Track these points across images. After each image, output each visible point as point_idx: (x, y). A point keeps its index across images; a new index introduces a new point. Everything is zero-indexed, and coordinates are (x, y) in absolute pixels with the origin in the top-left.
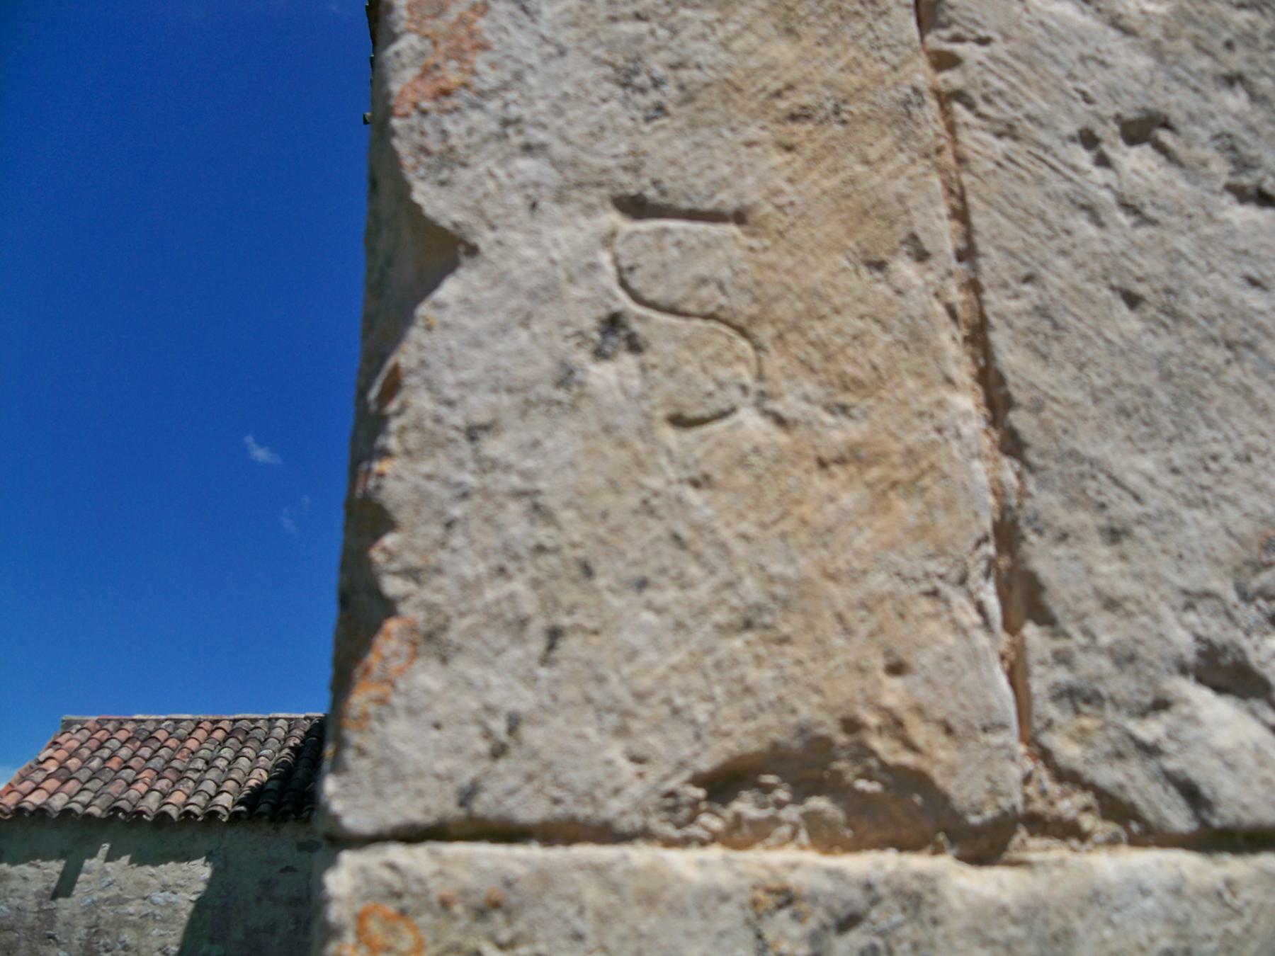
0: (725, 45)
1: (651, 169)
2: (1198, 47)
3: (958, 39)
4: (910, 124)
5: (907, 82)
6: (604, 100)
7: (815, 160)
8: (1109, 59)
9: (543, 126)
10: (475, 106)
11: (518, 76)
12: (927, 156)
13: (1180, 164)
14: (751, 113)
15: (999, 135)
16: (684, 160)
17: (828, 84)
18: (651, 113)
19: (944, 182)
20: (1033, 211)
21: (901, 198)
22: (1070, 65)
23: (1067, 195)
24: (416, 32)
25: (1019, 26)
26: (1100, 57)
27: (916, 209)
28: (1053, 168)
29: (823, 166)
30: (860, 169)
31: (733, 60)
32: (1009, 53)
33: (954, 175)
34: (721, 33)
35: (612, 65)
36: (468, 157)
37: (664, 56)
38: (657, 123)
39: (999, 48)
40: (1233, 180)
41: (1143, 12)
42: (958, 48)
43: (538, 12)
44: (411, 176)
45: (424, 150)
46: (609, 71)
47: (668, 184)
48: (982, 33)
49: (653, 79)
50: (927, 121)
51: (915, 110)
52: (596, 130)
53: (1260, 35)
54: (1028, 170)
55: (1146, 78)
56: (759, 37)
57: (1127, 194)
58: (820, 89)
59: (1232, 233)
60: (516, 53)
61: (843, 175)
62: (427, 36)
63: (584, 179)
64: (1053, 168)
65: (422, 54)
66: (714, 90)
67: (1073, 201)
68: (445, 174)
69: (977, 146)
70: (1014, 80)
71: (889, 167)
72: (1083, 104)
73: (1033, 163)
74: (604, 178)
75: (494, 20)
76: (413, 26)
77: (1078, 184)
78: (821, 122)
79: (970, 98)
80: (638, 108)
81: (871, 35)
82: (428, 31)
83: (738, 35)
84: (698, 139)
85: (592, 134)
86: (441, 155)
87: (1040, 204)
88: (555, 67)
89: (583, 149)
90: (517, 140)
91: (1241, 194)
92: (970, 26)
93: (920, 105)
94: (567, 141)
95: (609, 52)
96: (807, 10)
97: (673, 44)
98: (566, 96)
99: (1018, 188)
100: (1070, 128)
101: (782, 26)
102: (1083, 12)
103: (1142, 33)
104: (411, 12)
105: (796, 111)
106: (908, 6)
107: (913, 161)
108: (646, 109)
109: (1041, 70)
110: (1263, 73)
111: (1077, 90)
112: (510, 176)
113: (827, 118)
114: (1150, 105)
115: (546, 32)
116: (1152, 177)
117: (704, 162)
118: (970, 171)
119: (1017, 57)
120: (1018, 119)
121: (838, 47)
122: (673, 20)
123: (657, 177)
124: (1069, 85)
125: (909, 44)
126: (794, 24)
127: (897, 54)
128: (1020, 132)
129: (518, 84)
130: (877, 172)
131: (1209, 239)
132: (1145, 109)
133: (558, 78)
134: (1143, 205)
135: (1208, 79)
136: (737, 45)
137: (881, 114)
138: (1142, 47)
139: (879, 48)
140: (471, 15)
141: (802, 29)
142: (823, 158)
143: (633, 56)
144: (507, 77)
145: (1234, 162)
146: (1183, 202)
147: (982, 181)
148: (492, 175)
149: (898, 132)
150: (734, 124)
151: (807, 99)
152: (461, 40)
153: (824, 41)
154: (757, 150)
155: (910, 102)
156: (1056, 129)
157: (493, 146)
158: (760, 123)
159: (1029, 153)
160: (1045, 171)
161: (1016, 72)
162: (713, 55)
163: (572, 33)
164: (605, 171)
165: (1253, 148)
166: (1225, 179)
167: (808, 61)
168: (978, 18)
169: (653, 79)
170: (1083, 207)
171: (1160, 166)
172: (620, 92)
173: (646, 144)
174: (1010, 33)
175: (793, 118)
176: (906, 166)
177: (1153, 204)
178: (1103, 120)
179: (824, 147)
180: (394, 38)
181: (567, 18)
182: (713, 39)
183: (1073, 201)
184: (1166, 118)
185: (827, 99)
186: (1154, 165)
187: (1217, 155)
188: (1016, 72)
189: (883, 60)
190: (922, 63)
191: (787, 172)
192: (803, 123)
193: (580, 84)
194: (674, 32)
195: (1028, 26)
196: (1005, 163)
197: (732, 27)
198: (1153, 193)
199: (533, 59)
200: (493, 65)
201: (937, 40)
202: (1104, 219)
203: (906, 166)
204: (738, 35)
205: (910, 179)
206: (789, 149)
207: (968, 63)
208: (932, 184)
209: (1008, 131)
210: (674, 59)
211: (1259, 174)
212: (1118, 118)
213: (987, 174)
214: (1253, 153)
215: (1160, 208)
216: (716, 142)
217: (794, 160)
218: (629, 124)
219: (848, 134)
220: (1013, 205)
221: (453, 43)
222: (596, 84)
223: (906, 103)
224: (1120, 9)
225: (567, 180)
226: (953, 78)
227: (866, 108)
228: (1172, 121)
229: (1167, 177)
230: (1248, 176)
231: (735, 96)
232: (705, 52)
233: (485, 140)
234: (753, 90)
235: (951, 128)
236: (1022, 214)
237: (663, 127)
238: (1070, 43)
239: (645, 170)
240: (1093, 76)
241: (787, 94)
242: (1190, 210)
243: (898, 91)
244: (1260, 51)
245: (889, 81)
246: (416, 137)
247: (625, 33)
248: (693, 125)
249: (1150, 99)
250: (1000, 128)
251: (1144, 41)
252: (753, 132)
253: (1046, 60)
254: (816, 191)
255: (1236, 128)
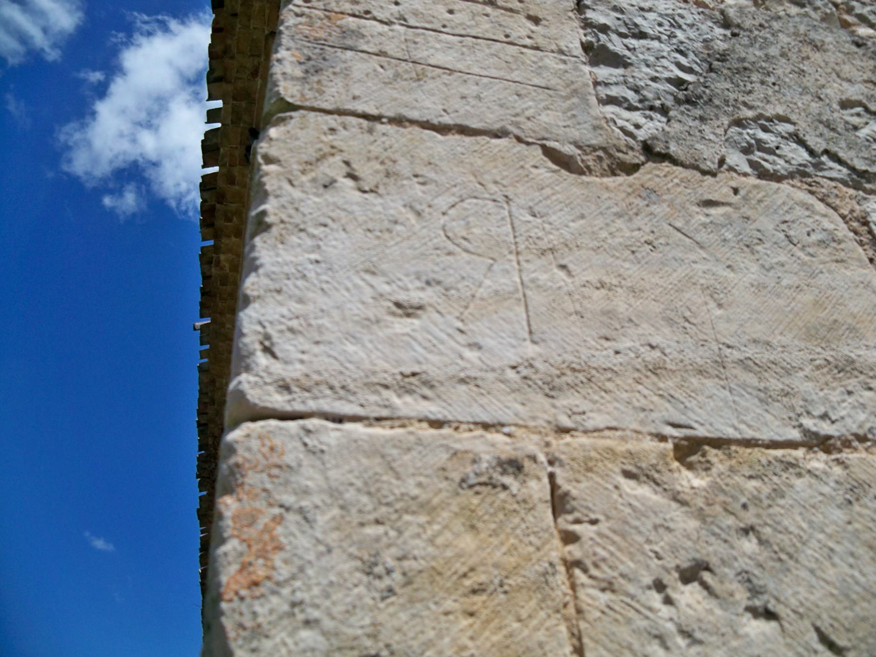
0: (431, 541)
1: (386, 635)
2: (726, 510)
3: (578, 521)
4: (547, 588)
5: (546, 559)
6: (356, 586)
7: (488, 621)
8: (671, 525)
9: (317, 606)
10: (274, 593)
11: (301, 569)
12: (558, 611)
13: (717, 597)
14: (448, 591)
15: (603, 590)
16: (405, 628)
17: (496, 566)
18: (385, 594)
19: (568, 628)
20: (625, 644)
21: (541, 645)
22: (648, 533)
23: (646, 630)
24: (237, 537)
25: (616, 508)
26: (666, 524)
27: (551, 651)
28: (637, 611)
29: (492, 625)
30: (516, 625)
31: (436, 552)
32: (610, 529)
33: (574, 622)
34: (429, 532)
35: (361, 559)
36: (269, 630)
37: (394, 551)
38: (389, 601)
39: (603, 527)
40: (750, 603)
41: (693, 488)
42: (577, 528)
43: (315, 521)
44: (233, 645)
45: (242, 626)
46: (358, 563)
47: (395, 647)
48: (593, 516)
49: (386, 569)
50: (558, 586)
51: (550, 579)
52: (350, 608)
53: (763, 497)
54: (621, 614)
55: (694, 536)
56: (453, 533)
57: (683, 624)
58: (491, 569)
59: (749, 644)
60: (300, 552)
61: (504, 632)
62: (244, 541)
63: (342, 645)
64: (637, 611)
65: (241, 554)
66: (425, 575)
67: (649, 633)
68: (254, 644)
69: (590, 601)
70: (612, 548)
71: (534, 622)
72: (656, 560)
73: (624, 608)
74: (355, 643)
75: (286, 527)
76: (236, 533)
77: (652, 620)
78: (491, 594)
79: (585, 565)
80: (376, 590)
81: (523, 526)
82: (245, 537)
83: (439, 533)
84: (414, 611)
85: (347, 612)
86: (253, 630)
87: (629, 639)
88: (325, 561)
89: (342, 622)
90: (300, 617)
91: (755, 612)
92: (585, 511)
93: (553, 574)
94: (333, 618)
95: (359, 549)
96: (484, 511)
97: (399, 541)
98: (331, 584)
99: (614, 628)
100: (648, 580)
101: (468, 523)
102: (656, 493)
103: (692, 503)
104: (235, 522)
105: (476, 587)
106: (546, 502)
107: (549, 616)
108: (382, 591)
109: (629, 540)
110: (766, 524)
111: (652, 551)
112: (296, 644)
113: (495, 590)
114: (698, 556)
115: (319, 535)
116: (699, 607)
117: (418, 629)
118: (584, 619)
119: (614, 532)
120: (614, 578)
121: (503, 536)
122: (399, 524)
123: (388, 641)
124: (647, 547)
125: (547, 530)
126: (475, 522)
127: (540, 538)
128: (616, 587)
129: (301, 575)
130: (527, 626)
131: (735, 650)
132: (694, 559)
133: (326, 570)
134: (693, 630)
135: (733, 532)
136: (439, 541)
137: (529, 584)
138: (692, 513)
139: (528, 535)
140: (272, 525)
141: (480, 525)
142: (493, 620)
143: (373, 552)
144: (295, 570)
145: (750, 590)
146: (719, 625)
147: (592, 626)
148: (285, 644)
149: (539, 596)
150: (437, 599)
151: (483, 578)
152: (265, 544)
153: (495, 533)
154: (451, 617)
155: (547, 573)
156: (639, 581)
157: (285, 622)
158: (453, 597)
159: (622, 601)
160: (632, 614)
161: (614, 543)
162: (424, 549)
163: (335, 535)
164: (356, 638)
165: (762, 579)
166: (745, 603)
167: (484, 549)
168: (590, 505)
169: (386, 569)
170: (656, 637)
171: (704, 598)
172: (365, 579)
173: (381, 618)
174: (610, 514)
175: (474, 592)
176: (545, 620)
177: (700, 628)
178: (668, 571)
179: (493, 612)
180: (223, 541)
181: (333, 524)
182: (424, 536)
183: (649, 633)
184: (708, 564)
185: (496, 577)
186: (700, 598)
187: (739, 586)
188: (614, 543)
189: (531, 543)
190: (557, 542)
191: (470, 633)
192: (480, 595)
193: (340, 574)
194: (400, 532)
195: (622, 508)
196: (607, 610)
197: (436, 527)
198: (700, 620)
199: (311, 556)
200: (286, 562)
201: (565, 522)
202: (669, 644)
203: (545, 620)
204: (439, 533)
205: (547, 629)
206: (472, 614)
207: (584, 539)
208: (560, 632)
209: (609, 587)
210: (400, 553)
211: (765, 597)
212: (678, 568)
213: (595, 620)
214: (761, 583)
215: (705, 631)
216: (425, 613)
217: (474, 623)
218: (371, 602)
219: (508, 600)
220: (612, 641)
221: (260, 546)
222: (351, 573)
223: (545, 574)
224: (679, 488)
225: (331, 645)
226: (575, 551)
227: (520, 580)
228: (711, 566)
229: (708, 607)
230: (759, 599)
231: (438, 578)
232: (418, 547)
233: (281, 618)
234: (449, 573)
235: (573, 587)
236: (617, 647)
237: (392, 604)
238: (647, 517)
239: (381, 637)
240: (662, 539)
241: (471, 574)
242: (723, 630)
243: (540, 566)
244: (763, 508)
245: (535, 557)
246: (237, 617)
247: (369, 535)
248: (411, 601)
249: (698, 551)
250: (604, 585)
251: (693, 509)
252: (449, 604)
253: (633, 531)
254: (488, 645)
255: (750, 565)
